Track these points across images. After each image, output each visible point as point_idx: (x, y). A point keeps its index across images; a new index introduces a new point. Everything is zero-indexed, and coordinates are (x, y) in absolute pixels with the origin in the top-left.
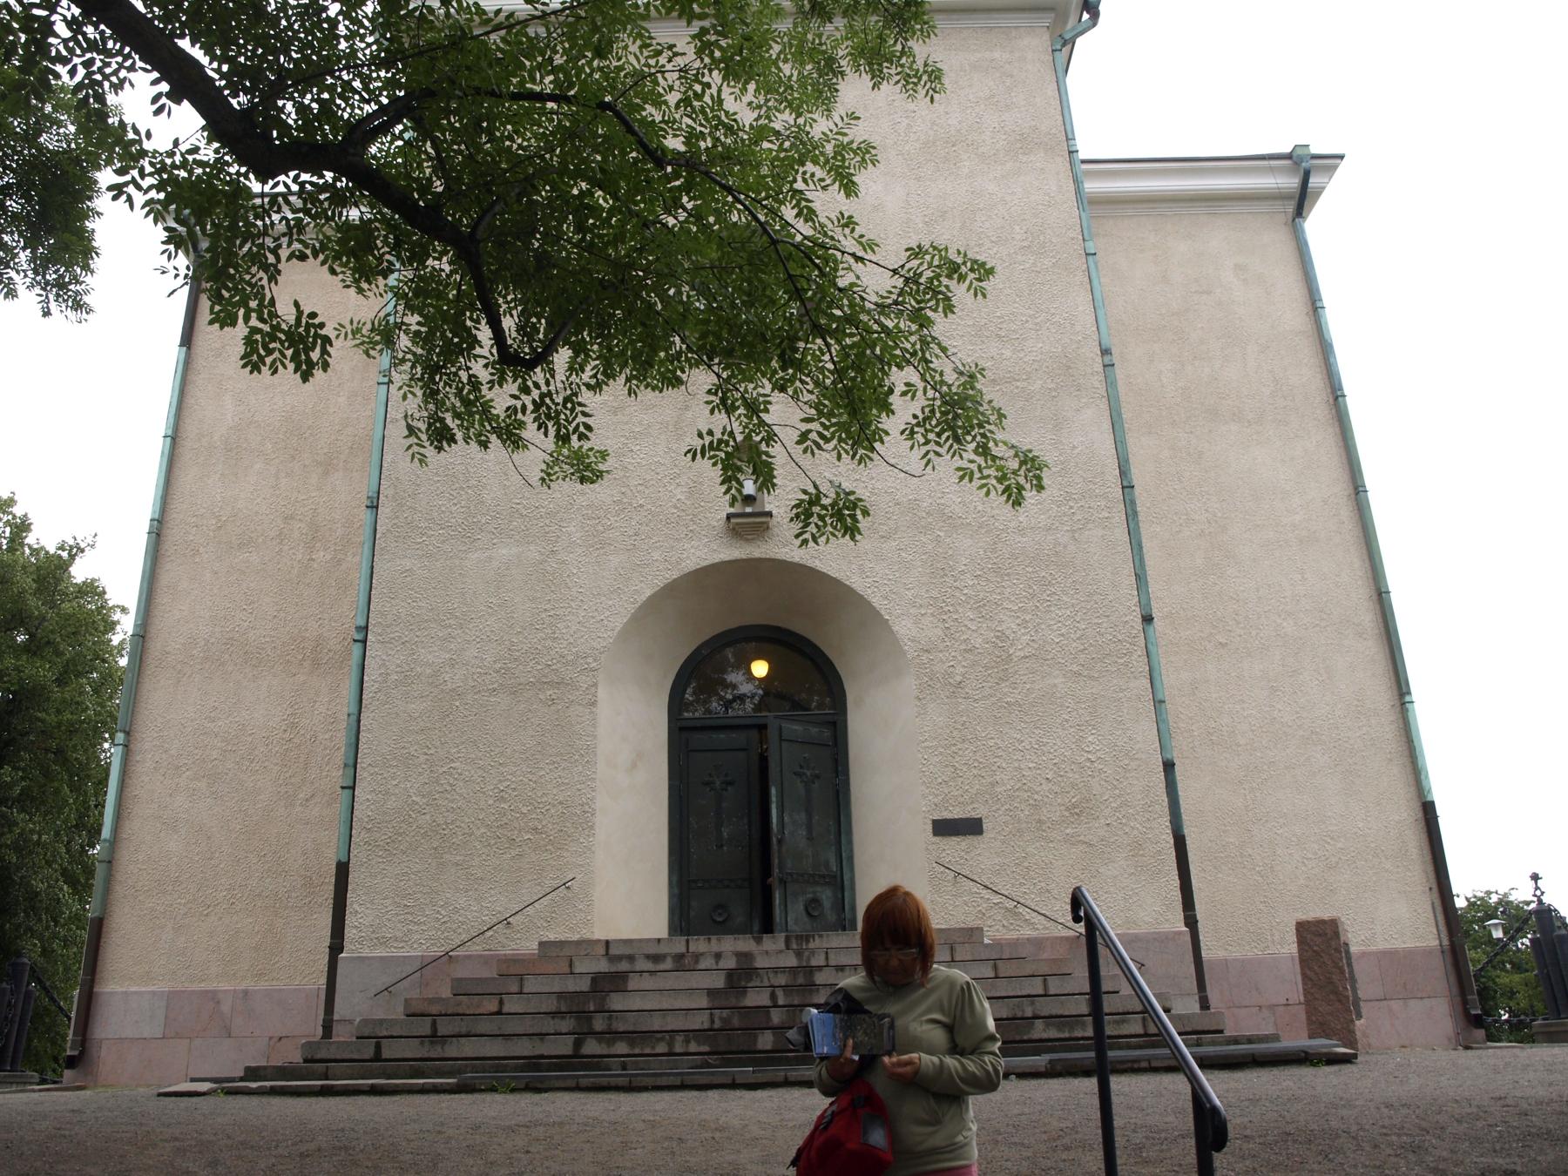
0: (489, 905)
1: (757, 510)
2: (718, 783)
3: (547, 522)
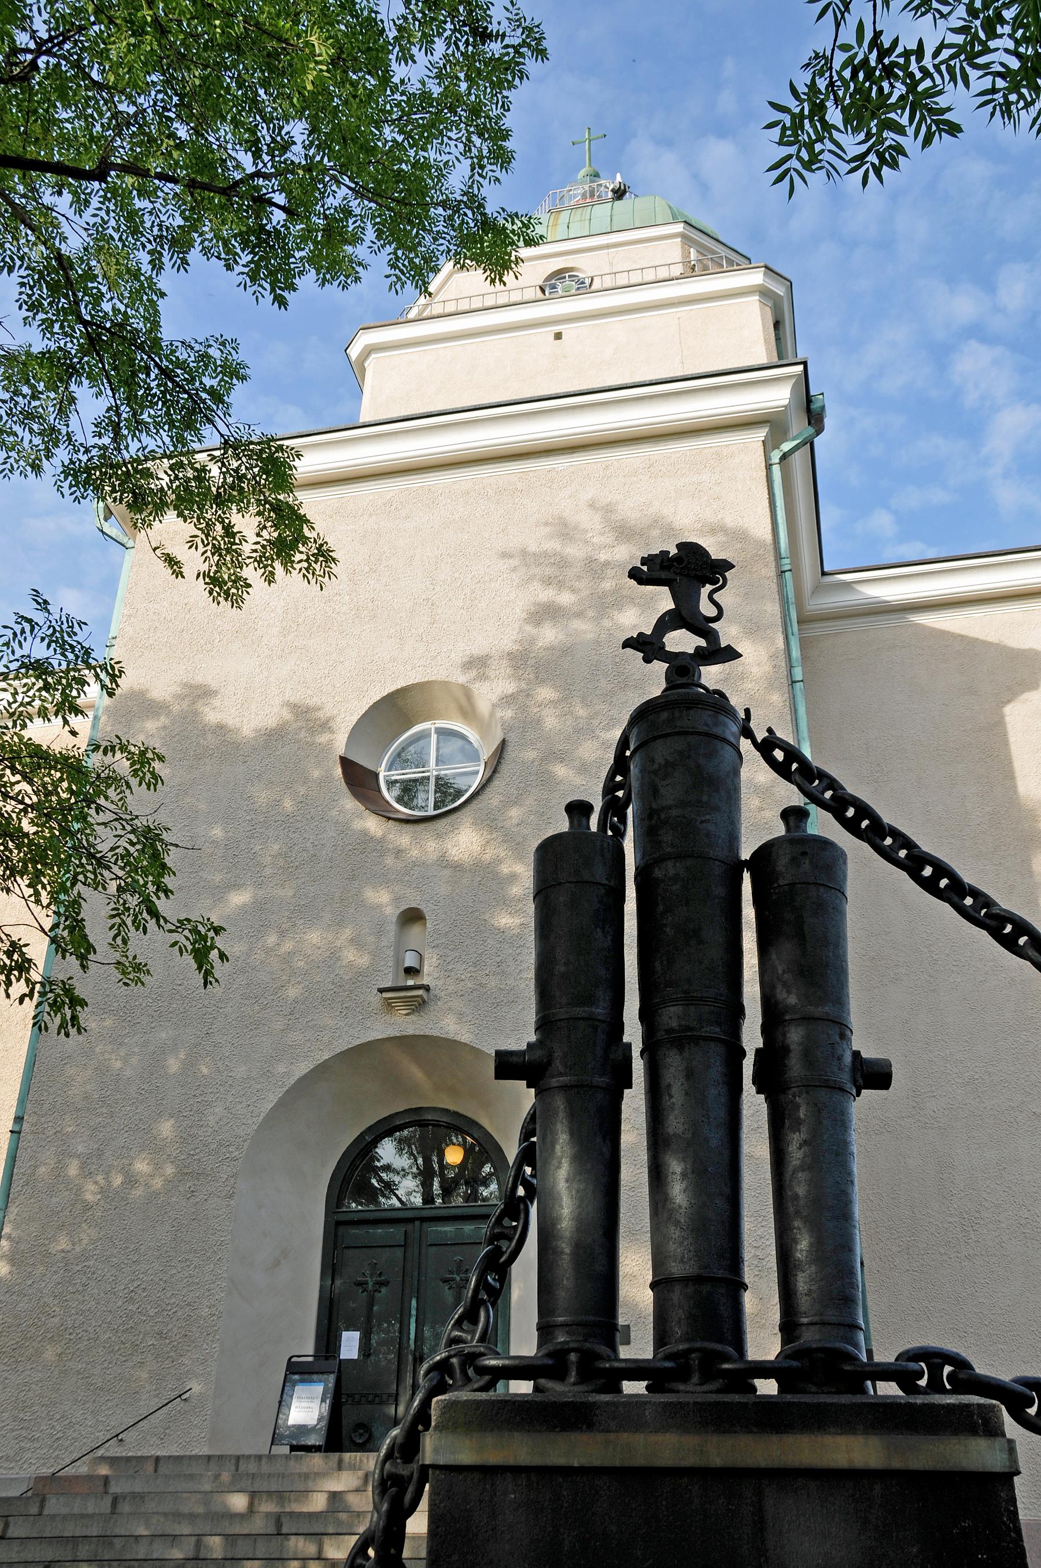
0: (104, 1419)
1: (418, 983)
2: (371, 1284)
3: (206, 1003)
